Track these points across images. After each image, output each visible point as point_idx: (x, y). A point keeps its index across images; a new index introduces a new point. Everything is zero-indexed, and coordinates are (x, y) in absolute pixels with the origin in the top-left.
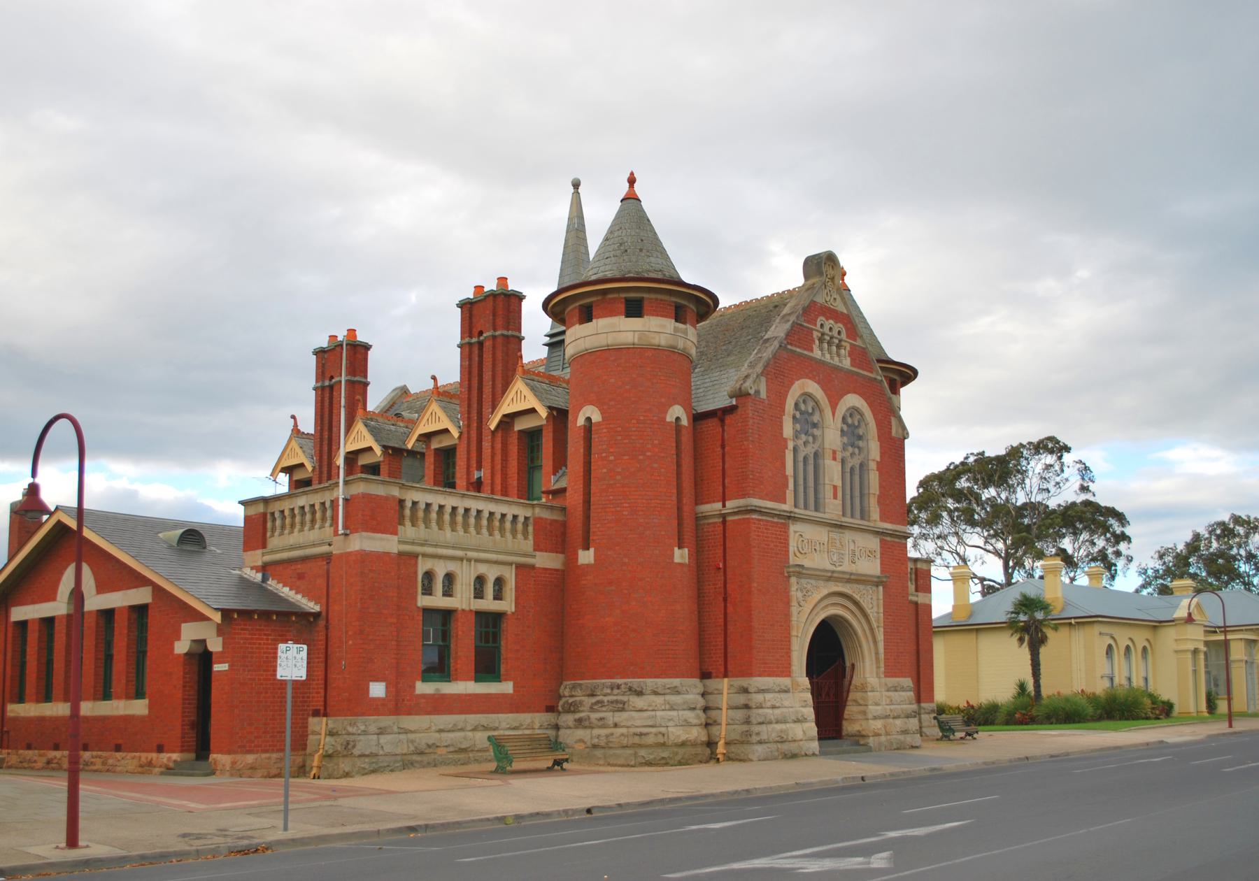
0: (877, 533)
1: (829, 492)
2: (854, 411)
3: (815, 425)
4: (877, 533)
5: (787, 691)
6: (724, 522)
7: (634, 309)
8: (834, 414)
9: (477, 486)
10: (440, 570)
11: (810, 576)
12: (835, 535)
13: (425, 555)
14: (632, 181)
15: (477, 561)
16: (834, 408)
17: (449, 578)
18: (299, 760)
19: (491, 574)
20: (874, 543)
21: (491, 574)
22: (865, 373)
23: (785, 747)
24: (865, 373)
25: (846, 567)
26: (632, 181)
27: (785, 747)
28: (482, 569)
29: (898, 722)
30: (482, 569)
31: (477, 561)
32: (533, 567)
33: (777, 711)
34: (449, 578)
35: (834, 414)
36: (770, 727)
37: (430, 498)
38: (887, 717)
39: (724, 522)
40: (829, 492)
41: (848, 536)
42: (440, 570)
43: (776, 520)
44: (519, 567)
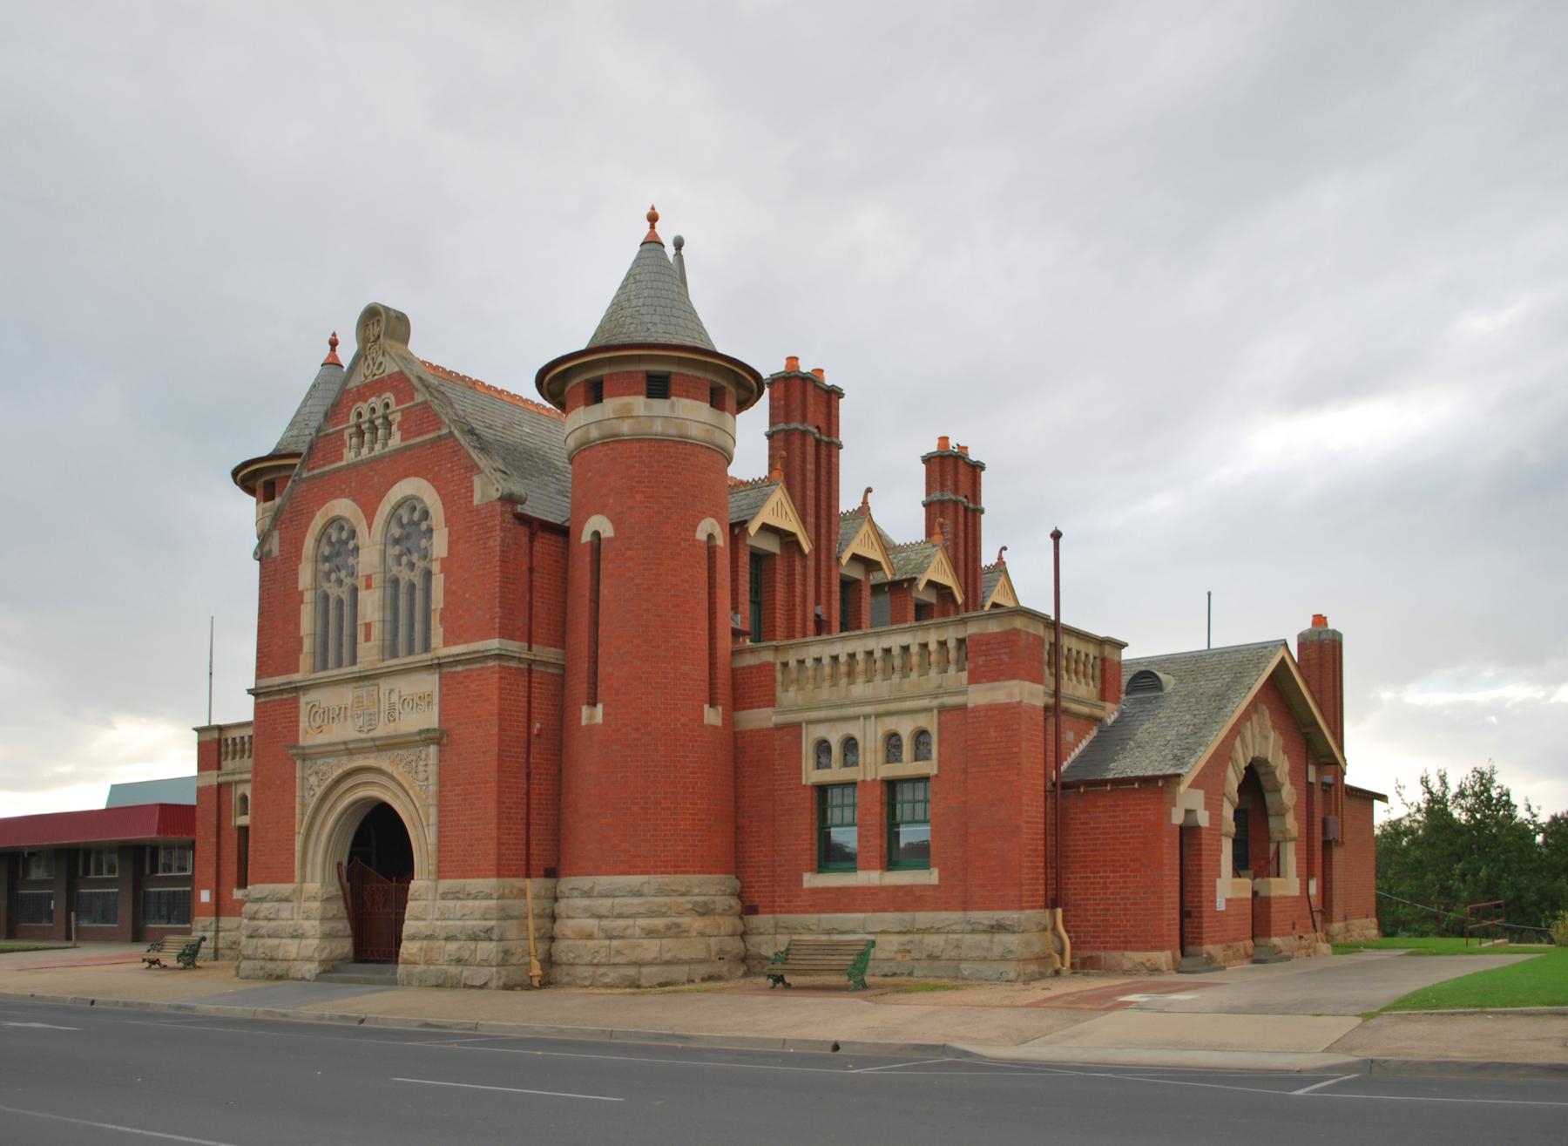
0: (430, 667)
1: (376, 631)
2: (409, 502)
3: (397, 541)
4: (430, 667)
5: (287, 900)
6: (530, 671)
7: (658, 387)
8: (370, 527)
9: (821, 626)
10: (835, 737)
11: (323, 755)
12: (365, 690)
13: (809, 722)
14: (653, 218)
15: (878, 716)
16: (370, 518)
17: (850, 744)
18: (1164, 968)
19: (906, 727)
20: (430, 683)
21: (906, 727)
22: (419, 439)
23: (270, 966)
24: (419, 439)
25: (383, 730)
26: (653, 218)
27: (270, 966)
28: (891, 724)
29: (452, 947)
30: (891, 724)
31: (878, 716)
32: (963, 708)
33: (273, 924)
34: (850, 744)
35: (370, 527)
36: (262, 941)
37: (887, 642)
38: (430, 937)
39: (530, 671)
40: (376, 631)
41: (385, 685)
42: (835, 737)
43: (285, 696)
44: (943, 709)
